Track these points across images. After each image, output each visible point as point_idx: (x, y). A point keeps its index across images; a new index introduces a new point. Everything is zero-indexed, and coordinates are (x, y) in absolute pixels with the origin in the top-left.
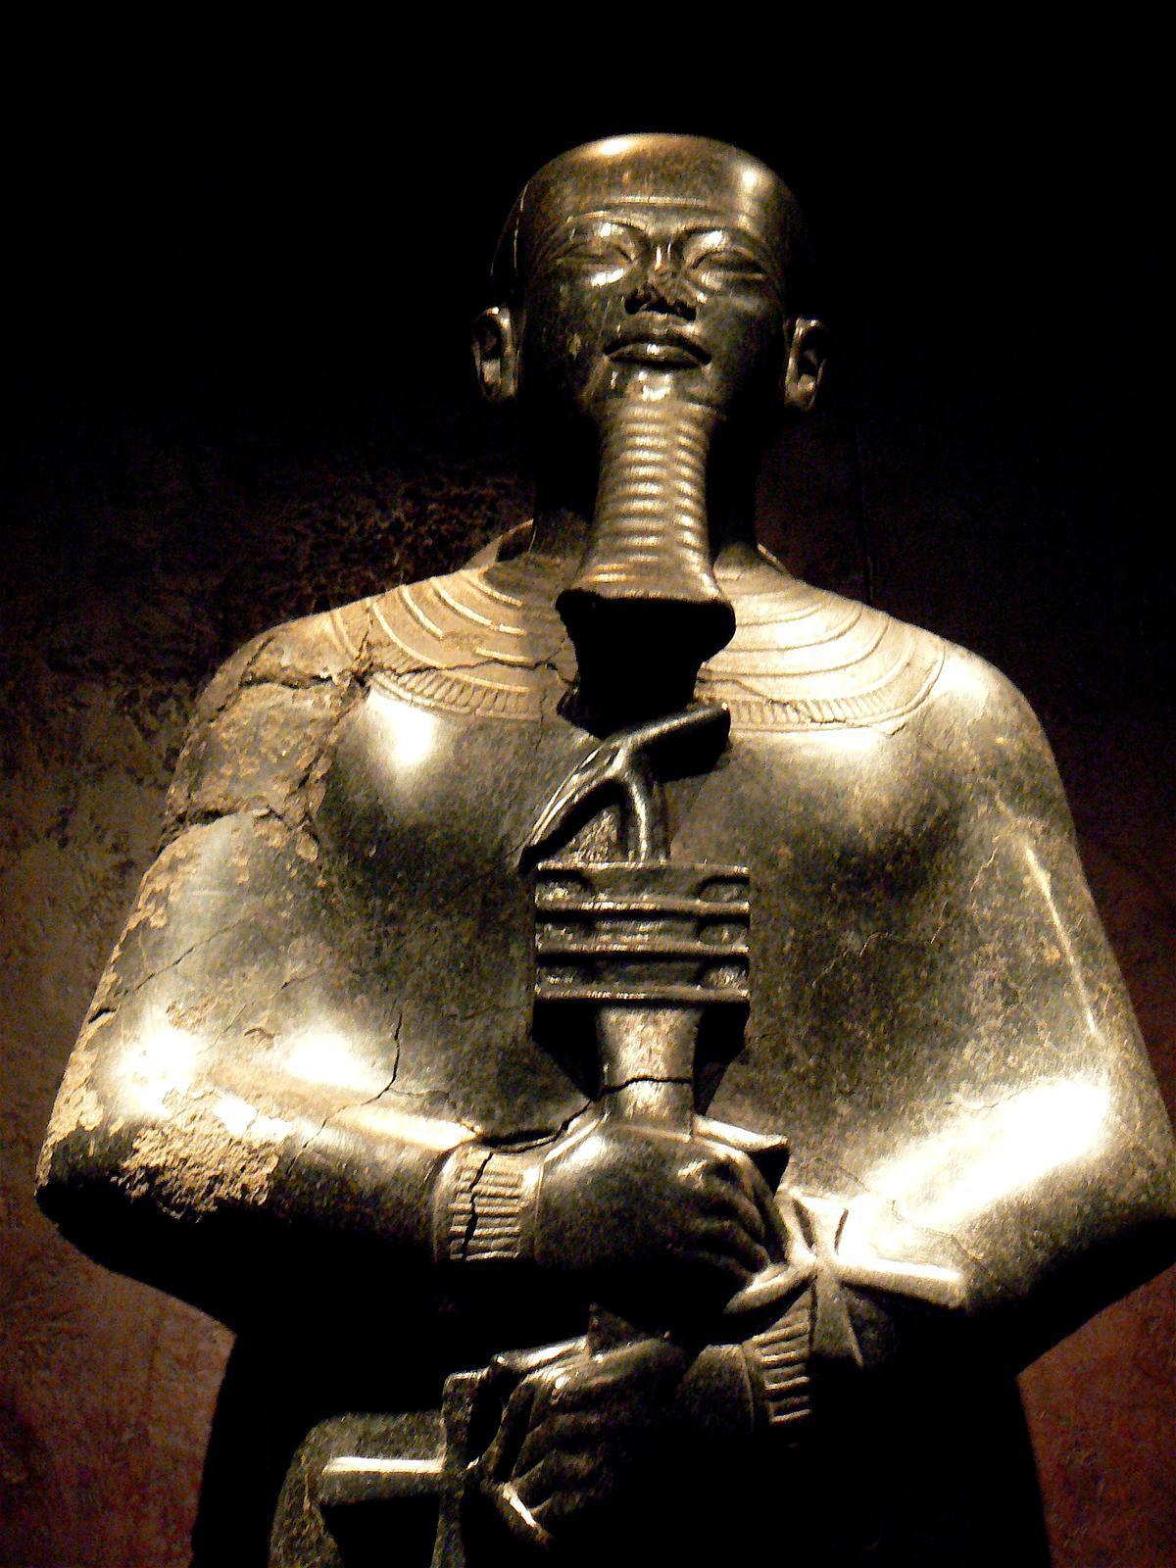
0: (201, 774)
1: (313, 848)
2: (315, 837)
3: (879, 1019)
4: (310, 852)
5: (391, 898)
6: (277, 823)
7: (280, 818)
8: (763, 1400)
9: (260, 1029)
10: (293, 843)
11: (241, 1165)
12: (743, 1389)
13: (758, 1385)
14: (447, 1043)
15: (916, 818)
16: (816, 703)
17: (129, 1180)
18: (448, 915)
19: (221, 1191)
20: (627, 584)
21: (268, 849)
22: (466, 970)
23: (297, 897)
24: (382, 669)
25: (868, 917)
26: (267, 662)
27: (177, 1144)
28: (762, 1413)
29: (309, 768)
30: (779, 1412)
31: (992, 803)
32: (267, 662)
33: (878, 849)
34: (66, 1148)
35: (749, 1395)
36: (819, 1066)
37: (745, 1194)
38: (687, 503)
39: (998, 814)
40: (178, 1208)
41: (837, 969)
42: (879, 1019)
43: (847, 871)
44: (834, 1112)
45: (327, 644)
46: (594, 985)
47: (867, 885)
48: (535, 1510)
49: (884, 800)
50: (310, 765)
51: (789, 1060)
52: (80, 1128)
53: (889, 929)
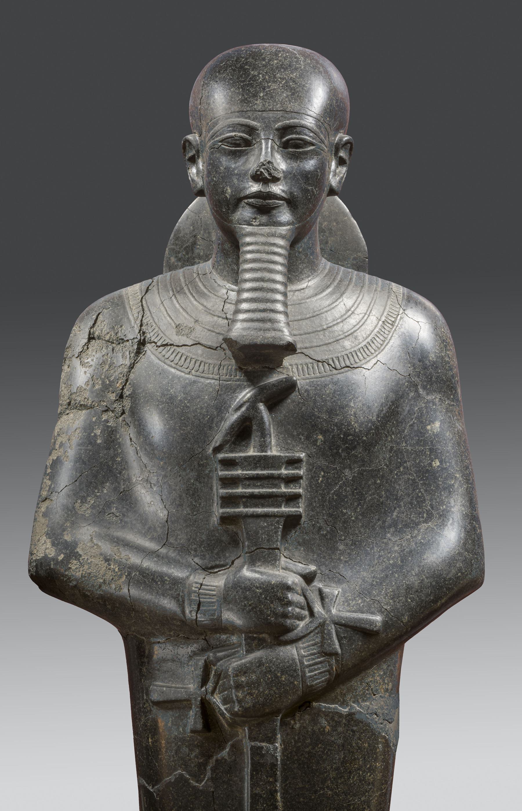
3: (358, 505)
6: (110, 413)
7: (113, 411)
8: (304, 668)
9: (113, 513)
11: (111, 578)
12: (296, 665)
13: (301, 663)
14: (187, 526)
15: (379, 410)
16: (338, 358)
17: (68, 579)
18: (185, 470)
22: (193, 494)
27: (86, 567)
28: (304, 673)
29: (123, 389)
30: (309, 672)
31: (417, 391)
33: (360, 431)
34: (41, 563)
35: (299, 667)
36: (331, 530)
37: (298, 594)
38: (279, 268)
39: (419, 396)
41: (341, 487)
42: (358, 505)
43: (346, 443)
44: (337, 549)
45: (160, 689)
46: (264, 378)
48: (225, 707)
50: (123, 386)
51: (320, 528)
53: (363, 465)
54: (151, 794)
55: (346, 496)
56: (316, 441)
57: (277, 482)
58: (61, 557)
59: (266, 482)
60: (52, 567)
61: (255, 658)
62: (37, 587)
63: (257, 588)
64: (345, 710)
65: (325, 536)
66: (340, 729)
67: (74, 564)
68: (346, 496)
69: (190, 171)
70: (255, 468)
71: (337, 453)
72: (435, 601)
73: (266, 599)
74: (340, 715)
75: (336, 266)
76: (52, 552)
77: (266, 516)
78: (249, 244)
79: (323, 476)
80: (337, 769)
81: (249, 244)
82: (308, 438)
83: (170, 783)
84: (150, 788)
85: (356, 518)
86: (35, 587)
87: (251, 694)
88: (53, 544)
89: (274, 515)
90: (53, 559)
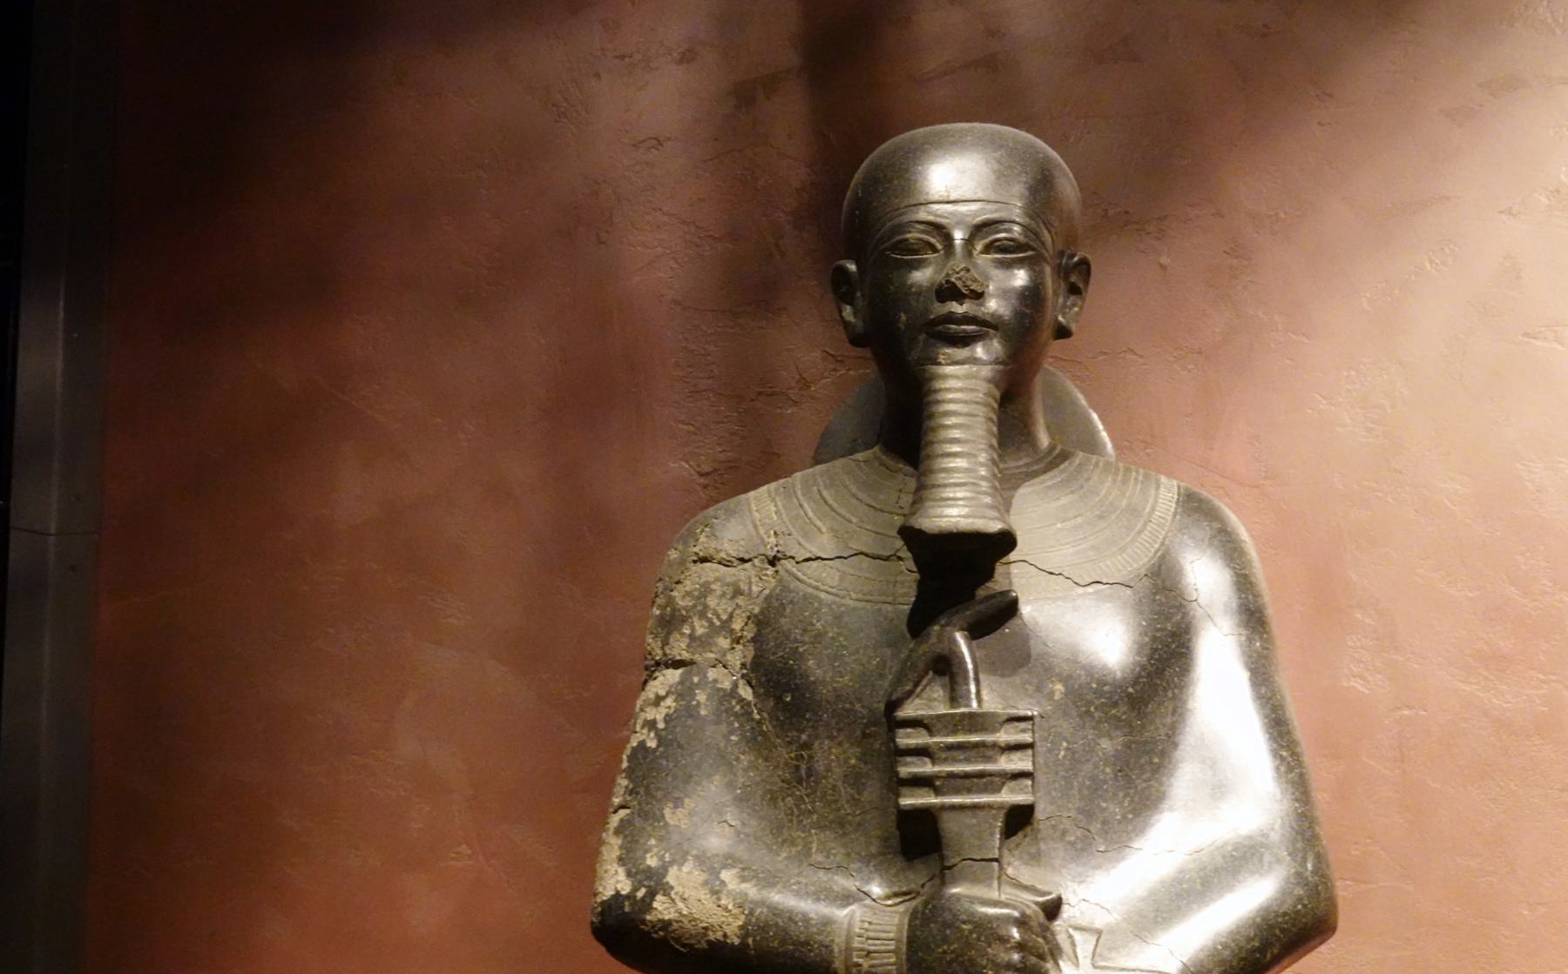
0: (669, 633)
1: (749, 690)
2: (749, 683)
4: (746, 693)
5: (803, 731)
10: (735, 685)
18: (840, 744)
19: (712, 937)
20: (982, 211)
21: (719, 690)
23: (741, 725)
24: (786, 558)
25: (1117, 728)
26: (704, 544)
32: (704, 544)
40: (684, 946)
47: (1115, 705)
49: (1119, 674)
51: (1064, 833)
52: (618, 893)
55: (1105, 782)
56: (1052, 693)
57: (990, 753)
58: (641, 894)
59: (973, 753)
60: (627, 909)
61: (1250, 561)
62: (602, 949)
63: (964, 922)
65: (1073, 844)
67: (659, 903)
68: (1105, 782)
69: (878, 880)
70: (954, 732)
71: (1088, 712)
73: (978, 939)
76: (625, 887)
79: (1067, 749)
82: (1039, 689)
85: (1124, 817)
88: (629, 874)
89: (989, 806)
90: (628, 897)
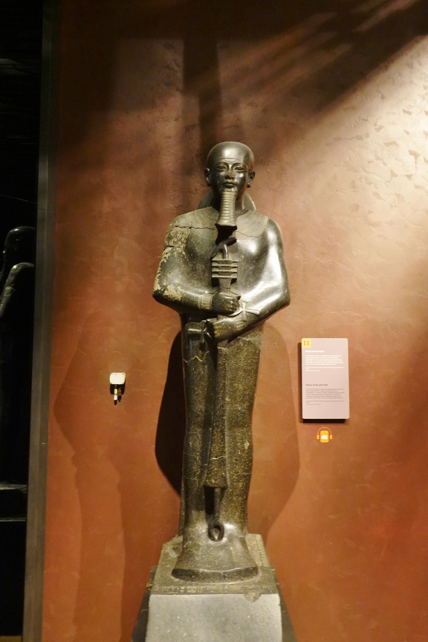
51: (242, 284)
54: (186, 363)
58: (162, 290)
64: (248, 340)
66: (246, 345)
70: (223, 264)
72: (276, 307)
74: (246, 341)
75: (282, 290)
76: (159, 289)
77: (226, 278)
78: (227, 207)
80: (244, 358)
81: (227, 207)
82: (239, 256)
83: (192, 360)
84: (186, 362)
86: (154, 299)
87: (219, 332)
88: (160, 286)
89: (228, 278)
90: (160, 290)
